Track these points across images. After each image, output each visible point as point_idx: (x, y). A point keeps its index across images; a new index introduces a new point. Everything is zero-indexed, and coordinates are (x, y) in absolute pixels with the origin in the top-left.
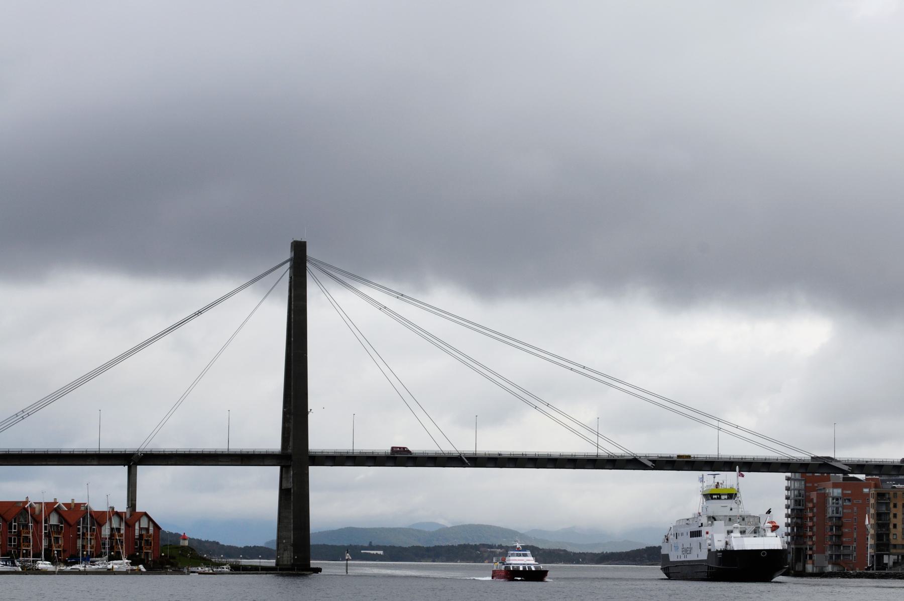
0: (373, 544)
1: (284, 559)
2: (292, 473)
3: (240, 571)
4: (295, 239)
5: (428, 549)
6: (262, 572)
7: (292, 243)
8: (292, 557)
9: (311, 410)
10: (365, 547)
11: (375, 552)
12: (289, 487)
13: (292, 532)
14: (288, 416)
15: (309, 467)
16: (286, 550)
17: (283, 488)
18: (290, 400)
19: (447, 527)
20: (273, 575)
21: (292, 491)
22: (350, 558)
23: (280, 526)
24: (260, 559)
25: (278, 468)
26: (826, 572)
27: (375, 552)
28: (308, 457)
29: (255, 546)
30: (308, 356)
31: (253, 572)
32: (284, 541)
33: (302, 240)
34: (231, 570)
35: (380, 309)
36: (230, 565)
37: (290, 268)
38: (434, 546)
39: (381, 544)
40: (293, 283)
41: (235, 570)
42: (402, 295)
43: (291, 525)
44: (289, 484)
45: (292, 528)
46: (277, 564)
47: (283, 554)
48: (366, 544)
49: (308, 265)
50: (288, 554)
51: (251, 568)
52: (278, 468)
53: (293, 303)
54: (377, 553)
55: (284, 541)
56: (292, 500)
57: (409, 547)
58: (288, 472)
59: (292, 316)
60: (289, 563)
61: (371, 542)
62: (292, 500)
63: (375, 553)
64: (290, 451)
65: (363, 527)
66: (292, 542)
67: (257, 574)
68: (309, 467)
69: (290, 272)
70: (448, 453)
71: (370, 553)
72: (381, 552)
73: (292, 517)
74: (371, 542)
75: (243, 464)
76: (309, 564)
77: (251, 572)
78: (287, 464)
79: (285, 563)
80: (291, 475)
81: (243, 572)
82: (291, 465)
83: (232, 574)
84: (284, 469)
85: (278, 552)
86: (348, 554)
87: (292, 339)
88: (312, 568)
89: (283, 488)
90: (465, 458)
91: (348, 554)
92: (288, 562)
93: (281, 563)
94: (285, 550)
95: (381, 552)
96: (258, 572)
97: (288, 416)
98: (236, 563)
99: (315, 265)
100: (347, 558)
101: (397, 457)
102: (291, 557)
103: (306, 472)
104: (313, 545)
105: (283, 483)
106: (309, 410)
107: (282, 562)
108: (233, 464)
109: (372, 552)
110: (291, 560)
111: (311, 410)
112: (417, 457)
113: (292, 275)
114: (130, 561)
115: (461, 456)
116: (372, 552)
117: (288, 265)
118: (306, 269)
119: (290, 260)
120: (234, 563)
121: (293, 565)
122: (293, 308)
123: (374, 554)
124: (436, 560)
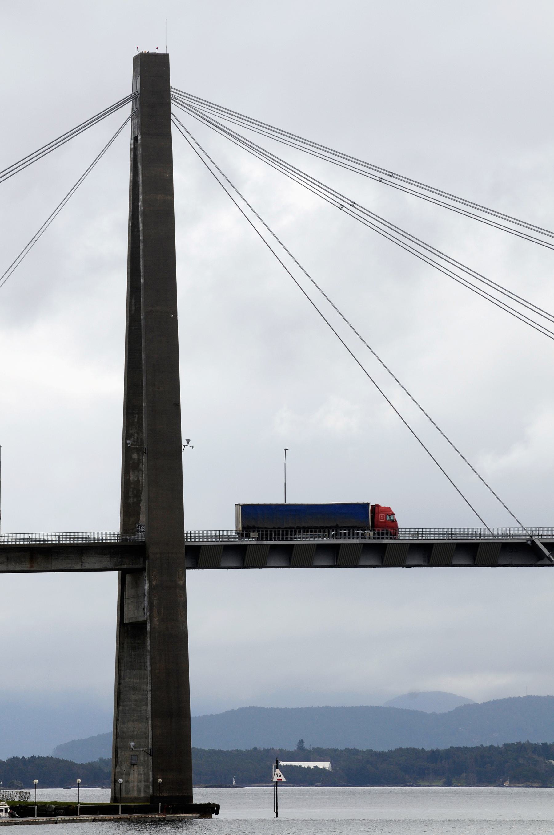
0: (307, 746)
1: (131, 785)
2: (147, 586)
3: (34, 817)
4: (142, 50)
5: (435, 755)
6: (85, 817)
7: (135, 59)
8: (151, 780)
9: (188, 441)
10: (289, 752)
11: (311, 765)
12: (142, 619)
13: (150, 722)
14: (135, 456)
15: (188, 572)
16: (137, 764)
17: (126, 621)
18: (140, 419)
19: (476, 705)
20: (115, 825)
21: (148, 628)
22: (284, 780)
23: (121, 708)
24: (79, 786)
25: (114, 576)
26: (331, 767)
27: (311, 765)
28: (184, 550)
29: (33, 757)
30: (179, 318)
31: (63, 818)
32: (132, 744)
33: (160, 52)
34: (11, 815)
35: (341, 207)
36: (8, 803)
37: (133, 116)
38: (448, 747)
39: (325, 746)
40: (139, 152)
41: (21, 815)
42: (391, 174)
43: (147, 705)
44: (141, 612)
45: (149, 714)
46: (114, 799)
47: (129, 774)
48: (292, 747)
49: (174, 108)
50: (139, 774)
51: (56, 809)
52: (114, 576)
53: (141, 197)
54: (316, 767)
55: (132, 744)
56: (149, 648)
57: (391, 752)
58: (137, 584)
59: (141, 228)
60: (142, 795)
61: (302, 742)
62: (149, 648)
63: (293, 765)
64: (140, 536)
65: (375, 705)
66: (150, 746)
67: (73, 821)
68: (188, 572)
69: (133, 125)
70: (504, 535)
71: (300, 767)
72: (326, 765)
73: (149, 687)
74: (302, 742)
75: (42, 569)
76: (190, 797)
77: (60, 818)
78: (137, 566)
79: (134, 794)
80: (146, 593)
81: (40, 819)
82: (143, 569)
83: (17, 824)
84: (128, 577)
85: (118, 769)
86: (278, 771)
87: (142, 281)
88: (196, 805)
89: (126, 621)
90: (543, 544)
91: (278, 771)
92: (139, 791)
93: (124, 795)
94: (132, 765)
95: (326, 765)
96: (75, 817)
97: (135, 456)
98: (21, 797)
99: (190, 109)
100: (275, 779)
101: (386, 544)
102: (147, 780)
103: (181, 583)
104: (202, 752)
105: (126, 609)
106: (184, 442)
107: (127, 792)
108: (11, 568)
109: (305, 764)
110: (147, 787)
111: (188, 441)
112: (432, 544)
113: (138, 132)
114: (9, 807)
115: (533, 542)
116: (305, 764)
117: (128, 110)
118: (170, 119)
119: (133, 98)
120: (16, 800)
121: (152, 799)
122: (141, 208)
123: (309, 768)
124: (454, 780)
